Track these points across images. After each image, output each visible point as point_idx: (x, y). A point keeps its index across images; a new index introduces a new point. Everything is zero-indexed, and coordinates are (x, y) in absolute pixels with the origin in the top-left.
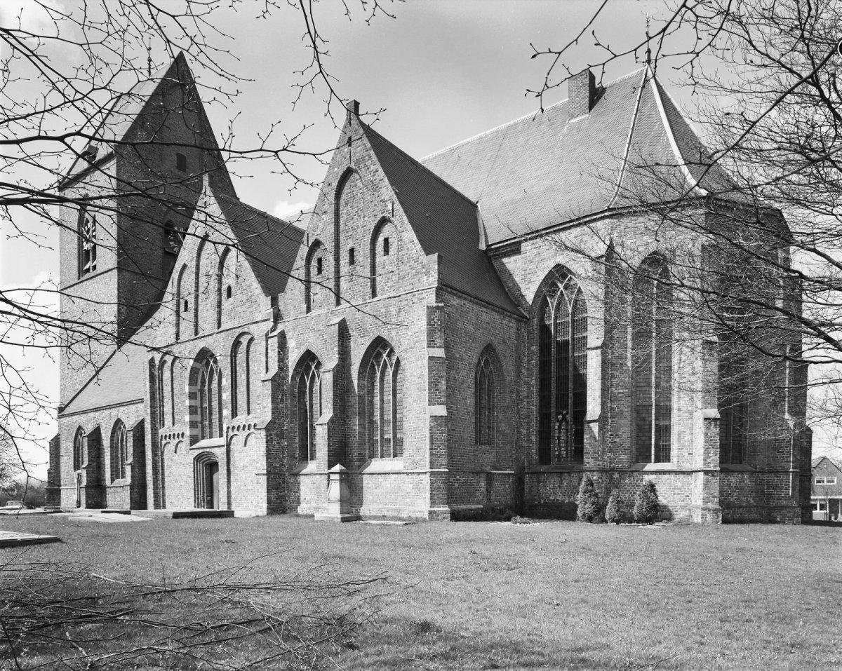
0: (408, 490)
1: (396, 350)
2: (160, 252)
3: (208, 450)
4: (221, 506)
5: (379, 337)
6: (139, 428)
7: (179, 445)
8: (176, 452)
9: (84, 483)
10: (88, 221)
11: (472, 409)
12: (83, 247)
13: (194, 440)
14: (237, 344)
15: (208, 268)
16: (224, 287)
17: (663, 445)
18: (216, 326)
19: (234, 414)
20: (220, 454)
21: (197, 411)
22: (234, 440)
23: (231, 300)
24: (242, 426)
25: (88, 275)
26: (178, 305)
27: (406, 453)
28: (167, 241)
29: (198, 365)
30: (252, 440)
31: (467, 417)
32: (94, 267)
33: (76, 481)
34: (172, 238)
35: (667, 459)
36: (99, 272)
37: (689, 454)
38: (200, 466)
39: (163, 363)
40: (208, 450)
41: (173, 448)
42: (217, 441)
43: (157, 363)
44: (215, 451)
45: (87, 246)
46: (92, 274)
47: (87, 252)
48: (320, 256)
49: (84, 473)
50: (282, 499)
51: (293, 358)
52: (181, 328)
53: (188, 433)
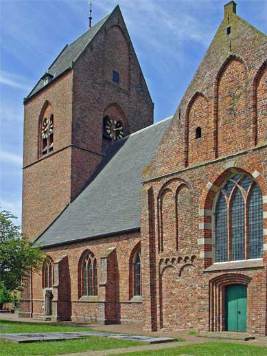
3: (242, 273)
7: (185, 269)
8: (180, 275)
9: (55, 298)
10: (46, 119)
12: (41, 137)
13: (208, 262)
15: (233, 91)
21: (211, 234)
25: (46, 155)
29: (216, 189)
34: (109, 128)
38: (216, 290)
39: (163, 191)
40: (242, 273)
41: (177, 271)
45: (44, 136)
47: (45, 140)
52: (190, 155)
53: (202, 255)
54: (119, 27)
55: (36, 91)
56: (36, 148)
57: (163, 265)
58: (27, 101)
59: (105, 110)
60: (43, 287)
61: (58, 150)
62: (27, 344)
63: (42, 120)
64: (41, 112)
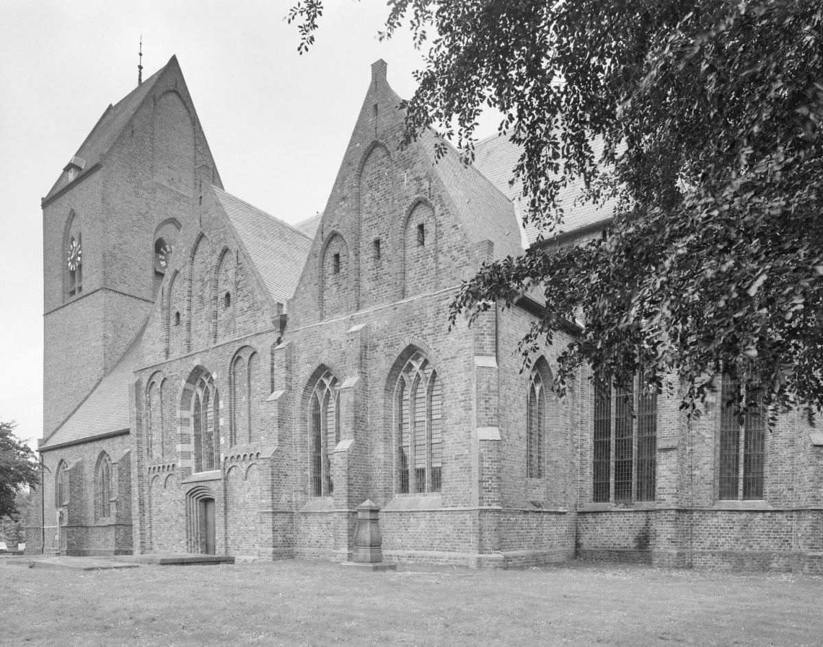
0: (448, 532)
1: (432, 362)
2: (150, 273)
3: (202, 484)
4: (220, 552)
5: (411, 345)
6: (126, 460)
11: (524, 434)
14: (236, 359)
15: (203, 274)
16: (173, 314)
17: (753, 478)
18: (212, 340)
19: (233, 441)
20: (215, 491)
21: (189, 439)
22: (232, 473)
23: (230, 309)
24: (229, 458)
25: (74, 298)
26: (168, 319)
27: (444, 487)
28: (158, 260)
29: (191, 387)
30: (255, 474)
31: (518, 443)
32: (80, 289)
33: (58, 520)
35: (759, 494)
36: (84, 294)
37: (789, 489)
39: (151, 384)
40: (202, 484)
41: (162, 483)
42: (216, 473)
43: (144, 385)
44: (213, 485)
45: (71, 267)
46: (77, 295)
47: (73, 273)
48: (336, 251)
49: (65, 512)
50: (289, 543)
51: (304, 372)
54: (177, 92)
55: (58, 190)
56: (60, 284)
57: (152, 476)
58: (46, 203)
59: (158, 229)
60: (56, 506)
61: (89, 291)
62: (187, 567)
63: (68, 239)
64: (66, 227)
